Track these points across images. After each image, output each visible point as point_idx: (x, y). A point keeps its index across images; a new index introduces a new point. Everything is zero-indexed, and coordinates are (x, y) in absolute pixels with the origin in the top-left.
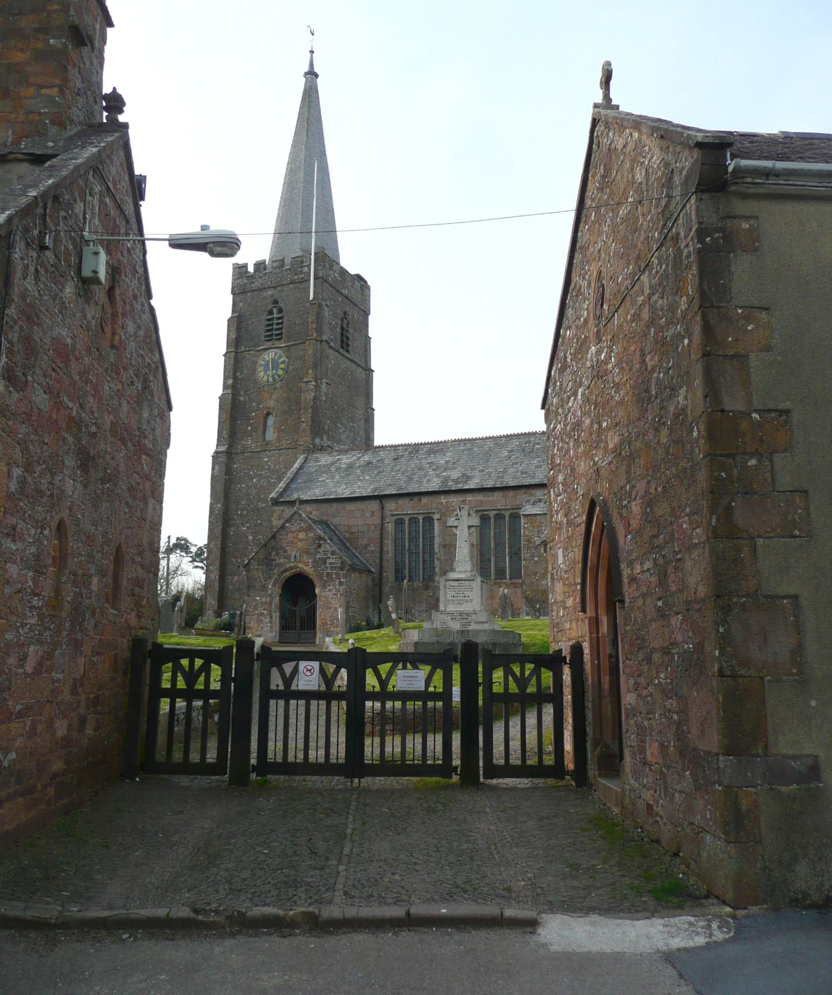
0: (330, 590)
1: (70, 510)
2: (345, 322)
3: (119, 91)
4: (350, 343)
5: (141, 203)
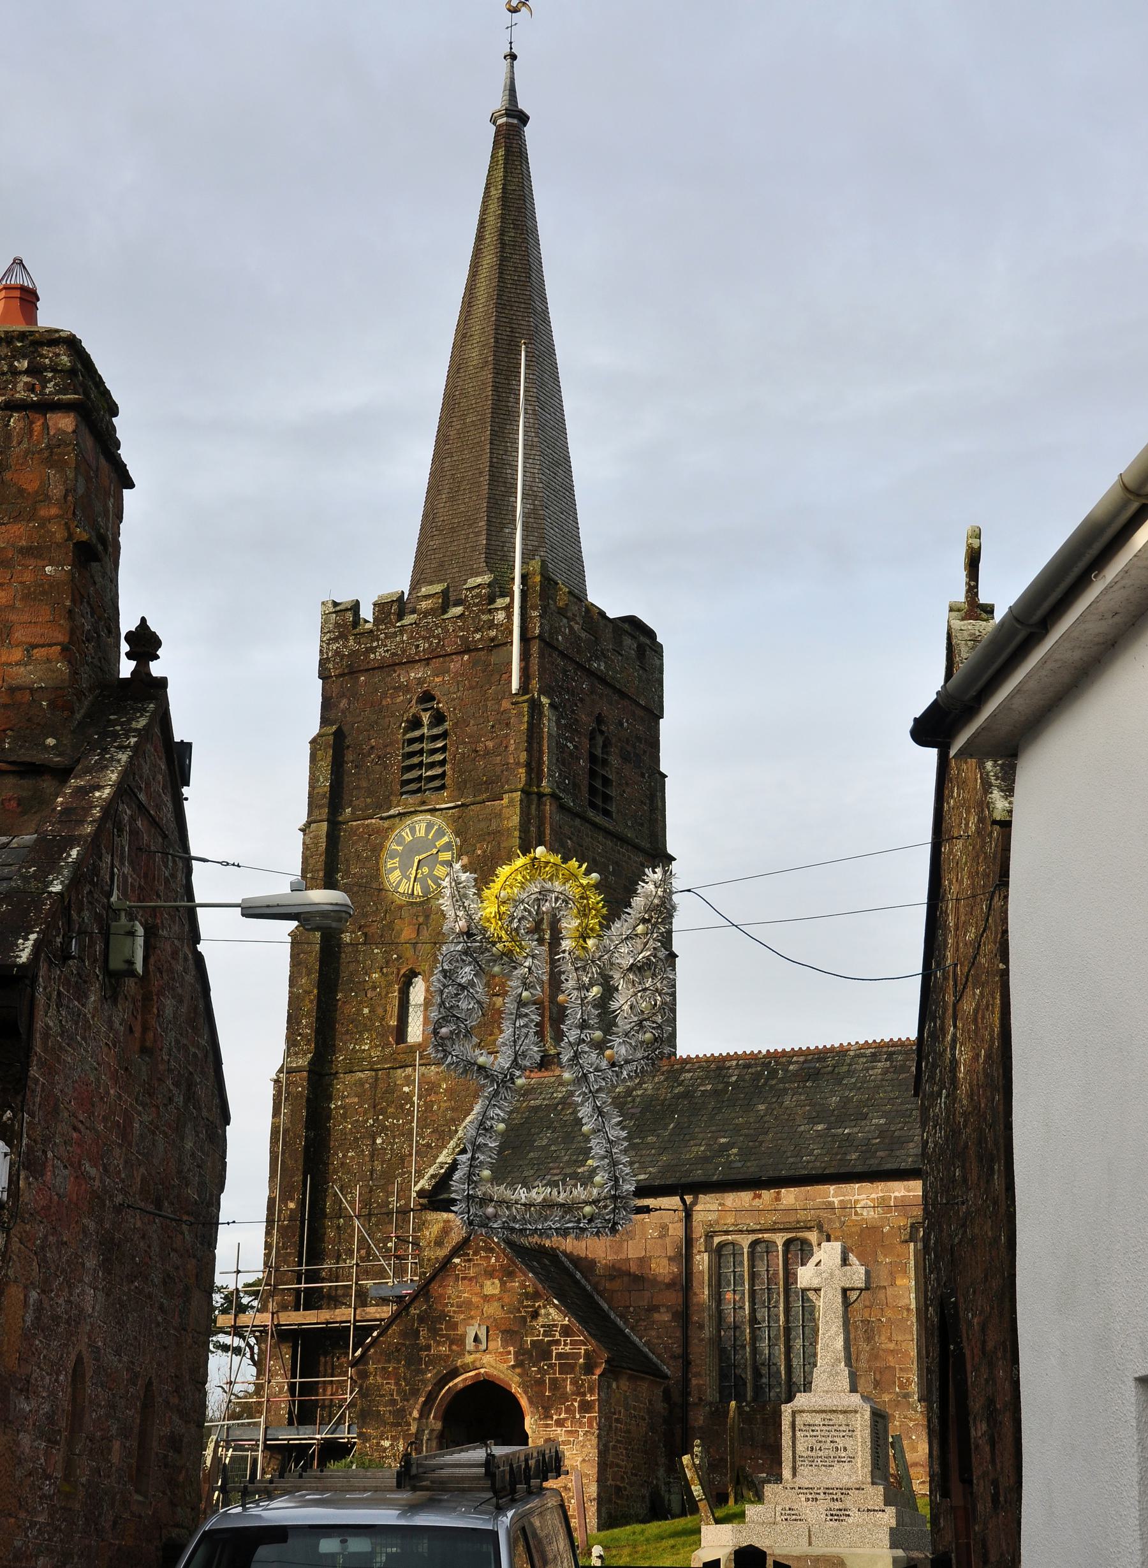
0: (560, 1423)
1: (89, 1338)
2: (600, 740)
3: (153, 627)
4: (613, 792)
5: (185, 791)
